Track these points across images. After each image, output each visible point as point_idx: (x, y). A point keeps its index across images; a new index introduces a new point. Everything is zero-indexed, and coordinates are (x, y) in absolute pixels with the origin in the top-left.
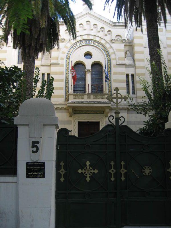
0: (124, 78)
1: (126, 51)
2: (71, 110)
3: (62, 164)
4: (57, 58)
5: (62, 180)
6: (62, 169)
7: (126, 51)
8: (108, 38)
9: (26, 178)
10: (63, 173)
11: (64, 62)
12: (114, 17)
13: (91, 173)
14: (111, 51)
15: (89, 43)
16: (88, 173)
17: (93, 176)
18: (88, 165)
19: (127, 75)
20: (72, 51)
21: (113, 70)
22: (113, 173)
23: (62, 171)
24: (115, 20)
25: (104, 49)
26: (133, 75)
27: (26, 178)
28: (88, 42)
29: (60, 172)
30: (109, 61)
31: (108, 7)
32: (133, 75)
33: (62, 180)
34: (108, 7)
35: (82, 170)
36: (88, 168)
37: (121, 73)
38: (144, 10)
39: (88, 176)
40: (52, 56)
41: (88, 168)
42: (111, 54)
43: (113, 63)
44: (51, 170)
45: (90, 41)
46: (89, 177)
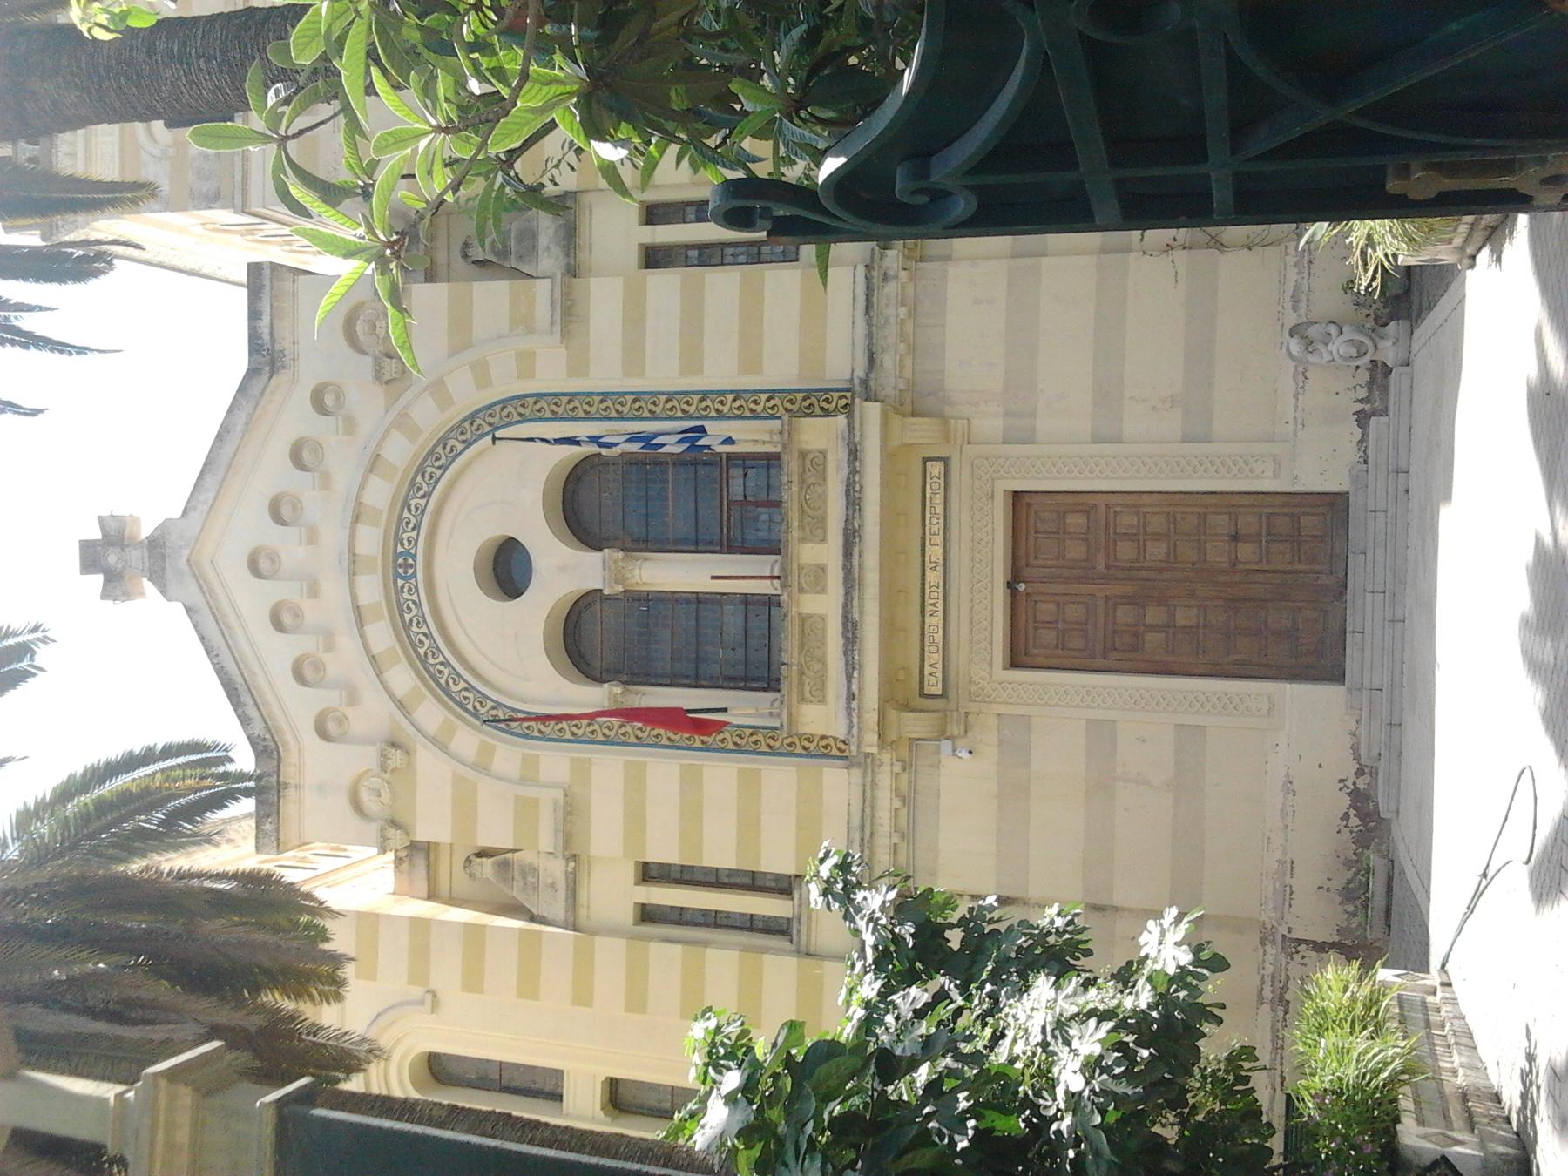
0: (666, 283)
1: (475, 262)
2: (914, 725)
4: (525, 811)
7: (475, 262)
8: (366, 402)
9: (249, 265)
11: (555, 762)
12: (47, 309)
14: (468, 396)
15: (414, 557)
19: (654, 258)
20: (470, 688)
21: (605, 375)
25: (452, 442)
26: (654, 214)
27: (249, 265)
28: (406, 566)
30: (543, 404)
32: (654, 214)
37: (635, 320)
38: (1139, 1108)
40: (511, 847)
42: (421, 440)
43: (552, 376)
45: (400, 549)
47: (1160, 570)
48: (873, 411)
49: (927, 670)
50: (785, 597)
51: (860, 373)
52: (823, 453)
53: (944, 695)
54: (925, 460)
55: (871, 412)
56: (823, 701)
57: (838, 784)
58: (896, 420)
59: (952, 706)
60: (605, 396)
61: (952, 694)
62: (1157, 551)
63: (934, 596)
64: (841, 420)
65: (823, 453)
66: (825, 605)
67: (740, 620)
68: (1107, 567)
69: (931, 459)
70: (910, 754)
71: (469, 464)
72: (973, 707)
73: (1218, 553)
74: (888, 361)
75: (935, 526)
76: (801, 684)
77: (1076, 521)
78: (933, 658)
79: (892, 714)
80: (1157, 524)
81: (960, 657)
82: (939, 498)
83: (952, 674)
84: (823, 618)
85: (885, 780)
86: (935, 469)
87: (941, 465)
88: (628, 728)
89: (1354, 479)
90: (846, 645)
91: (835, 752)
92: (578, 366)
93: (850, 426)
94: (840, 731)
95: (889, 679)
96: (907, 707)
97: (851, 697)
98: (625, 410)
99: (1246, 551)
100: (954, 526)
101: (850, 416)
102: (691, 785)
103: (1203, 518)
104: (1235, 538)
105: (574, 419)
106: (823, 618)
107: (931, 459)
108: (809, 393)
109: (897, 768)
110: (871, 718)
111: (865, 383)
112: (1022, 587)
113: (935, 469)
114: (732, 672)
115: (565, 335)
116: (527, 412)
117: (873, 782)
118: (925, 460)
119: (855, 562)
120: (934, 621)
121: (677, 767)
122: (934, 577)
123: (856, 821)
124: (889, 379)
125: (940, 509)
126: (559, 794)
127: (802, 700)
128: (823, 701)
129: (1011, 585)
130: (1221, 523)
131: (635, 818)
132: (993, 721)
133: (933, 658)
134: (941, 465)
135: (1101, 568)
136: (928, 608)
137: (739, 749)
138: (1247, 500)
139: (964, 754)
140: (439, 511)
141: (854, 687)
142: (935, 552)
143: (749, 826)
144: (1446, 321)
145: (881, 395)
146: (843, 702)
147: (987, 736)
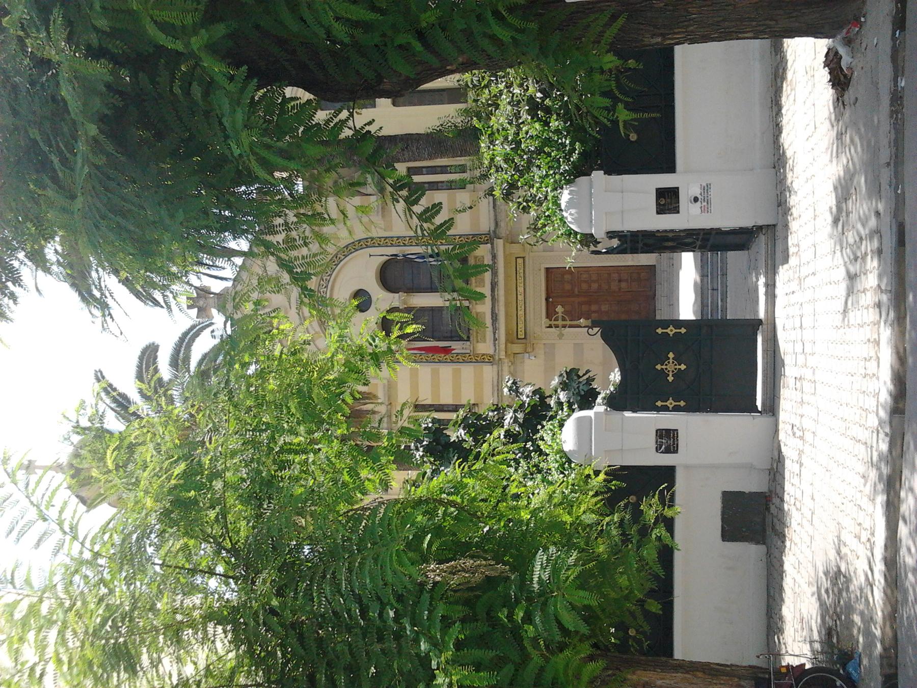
2: (517, 348)
3: (659, 404)
5: (682, 403)
6: (668, 403)
10: (669, 332)
13: (666, 365)
16: (668, 367)
17: (664, 374)
18: (671, 358)
22: (675, 331)
23: (671, 403)
24: (839, 324)
29: (671, 407)
31: (38, 544)
33: (682, 403)
34: (38, 544)
35: (673, 359)
36: (671, 362)
39: (664, 367)
41: (671, 362)
44: (667, 420)
46: (662, 369)
47: (596, 292)
48: (500, 242)
49: (519, 330)
50: (470, 307)
51: (492, 228)
52: (483, 257)
53: (525, 338)
54: (516, 258)
55: (499, 243)
56: (485, 342)
57: (488, 371)
58: (508, 245)
59: (528, 341)
60: (398, 238)
61: (528, 337)
62: (595, 286)
63: (521, 303)
64: (489, 245)
65: (483, 257)
66: (483, 308)
67: (97, 275)
68: (579, 292)
69: (524, 260)
70: (514, 357)
71: (347, 262)
72: (535, 342)
73: (614, 286)
74: (502, 224)
75: (520, 280)
76: (477, 336)
77: (567, 277)
78: (521, 325)
79: (509, 345)
80: (594, 277)
81: (530, 325)
82: (522, 271)
83: (528, 329)
84: (484, 313)
85: (506, 368)
86: (520, 261)
87: (522, 260)
88: (447, 357)
89: (657, 261)
90: (493, 322)
91: (487, 360)
92: (389, 227)
93: (492, 247)
94: (491, 352)
95: (508, 334)
96: (513, 343)
97: (495, 340)
98: (406, 242)
99: (623, 285)
100: (527, 281)
101: (492, 244)
102: (435, 376)
103: (609, 274)
104: (620, 281)
105: (387, 246)
106: (484, 313)
107: (524, 260)
108: (474, 235)
109: (510, 364)
110: (503, 347)
111: (494, 232)
112: (551, 300)
113: (520, 261)
114: (446, 335)
115: (383, 216)
116: (369, 244)
117: (502, 370)
118: (516, 258)
119: (496, 293)
120: (521, 313)
121: (430, 369)
122: (520, 298)
123: (495, 383)
124: (503, 231)
125: (522, 275)
126: (385, 382)
127: (478, 342)
128: (485, 342)
129: (547, 299)
130: (615, 276)
131: (415, 386)
132: (542, 346)
133: (521, 325)
134: (522, 260)
135: (576, 292)
136: (519, 308)
137: (452, 362)
138: (623, 268)
139: (533, 358)
140: (335, 280)
141: (497, 336)
142: (521, 289)
143: (435, 387)
144: (793, 292)
145: (501, 236)
146: (492, 341)
147: (540, 351)
